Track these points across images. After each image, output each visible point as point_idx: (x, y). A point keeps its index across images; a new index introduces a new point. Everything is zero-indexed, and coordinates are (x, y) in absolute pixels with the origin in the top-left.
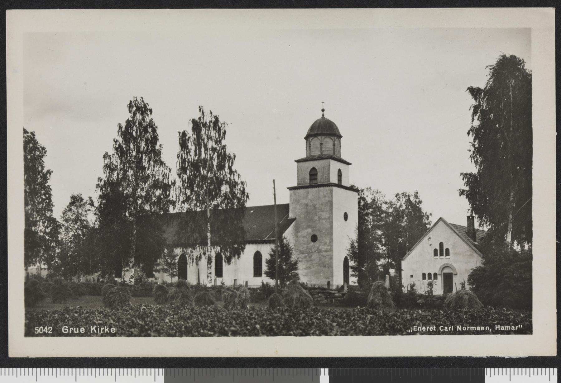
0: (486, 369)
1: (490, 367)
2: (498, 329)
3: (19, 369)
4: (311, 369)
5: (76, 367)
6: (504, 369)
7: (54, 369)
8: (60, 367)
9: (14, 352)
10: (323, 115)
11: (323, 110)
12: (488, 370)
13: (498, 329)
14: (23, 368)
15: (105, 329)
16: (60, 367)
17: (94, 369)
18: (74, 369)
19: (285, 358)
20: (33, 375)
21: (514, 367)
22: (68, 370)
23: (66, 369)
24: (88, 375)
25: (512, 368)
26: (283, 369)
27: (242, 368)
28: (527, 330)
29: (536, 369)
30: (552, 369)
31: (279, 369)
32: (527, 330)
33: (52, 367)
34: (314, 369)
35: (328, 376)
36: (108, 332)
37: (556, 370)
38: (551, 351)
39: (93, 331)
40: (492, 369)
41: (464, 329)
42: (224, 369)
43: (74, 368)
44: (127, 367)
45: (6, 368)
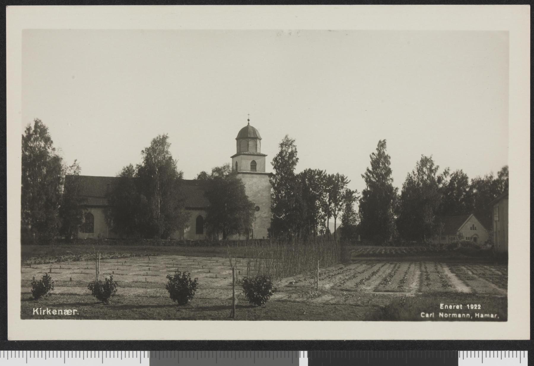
0: (459, 351)
1: (463, 349)
2: (477, 316)
3: (10, 352)
4: (290, 352)
5: (65, 350)
6: (477, 352)
7: (44, 352)
8: (49, 349)
9: (13, 335)
10: (249, 123)
11: (249, 120)
12: (461, 352)
13: (477, 316)
14: (14, 350)
15: (46, 310)
16: (50, 350)
17: (466, 352)
18: (63, 352)
19: (284, 340)
20: (471, 357)
21: (87, 349)
22: (27, 352)
23: (55, 352)
24: (475, 357)
25: (59, 350)
26: (264, 352)
27: (224, 350)
28: (503, 317)
29: (507, 352)
30: (522, 352)
31: (260, 352)
32: (503, 317)
33: (42, 349)
34: (214, 351)
35: (307, 359)
36: (50, 314)
37: (526, 352)
38: (526, 336)
39: (35, 312)
40: (465, 352)
41: (446, 315)
42: (207, 352)
43: (112, 350)
44: (114, 350)
45: (491, 350)
